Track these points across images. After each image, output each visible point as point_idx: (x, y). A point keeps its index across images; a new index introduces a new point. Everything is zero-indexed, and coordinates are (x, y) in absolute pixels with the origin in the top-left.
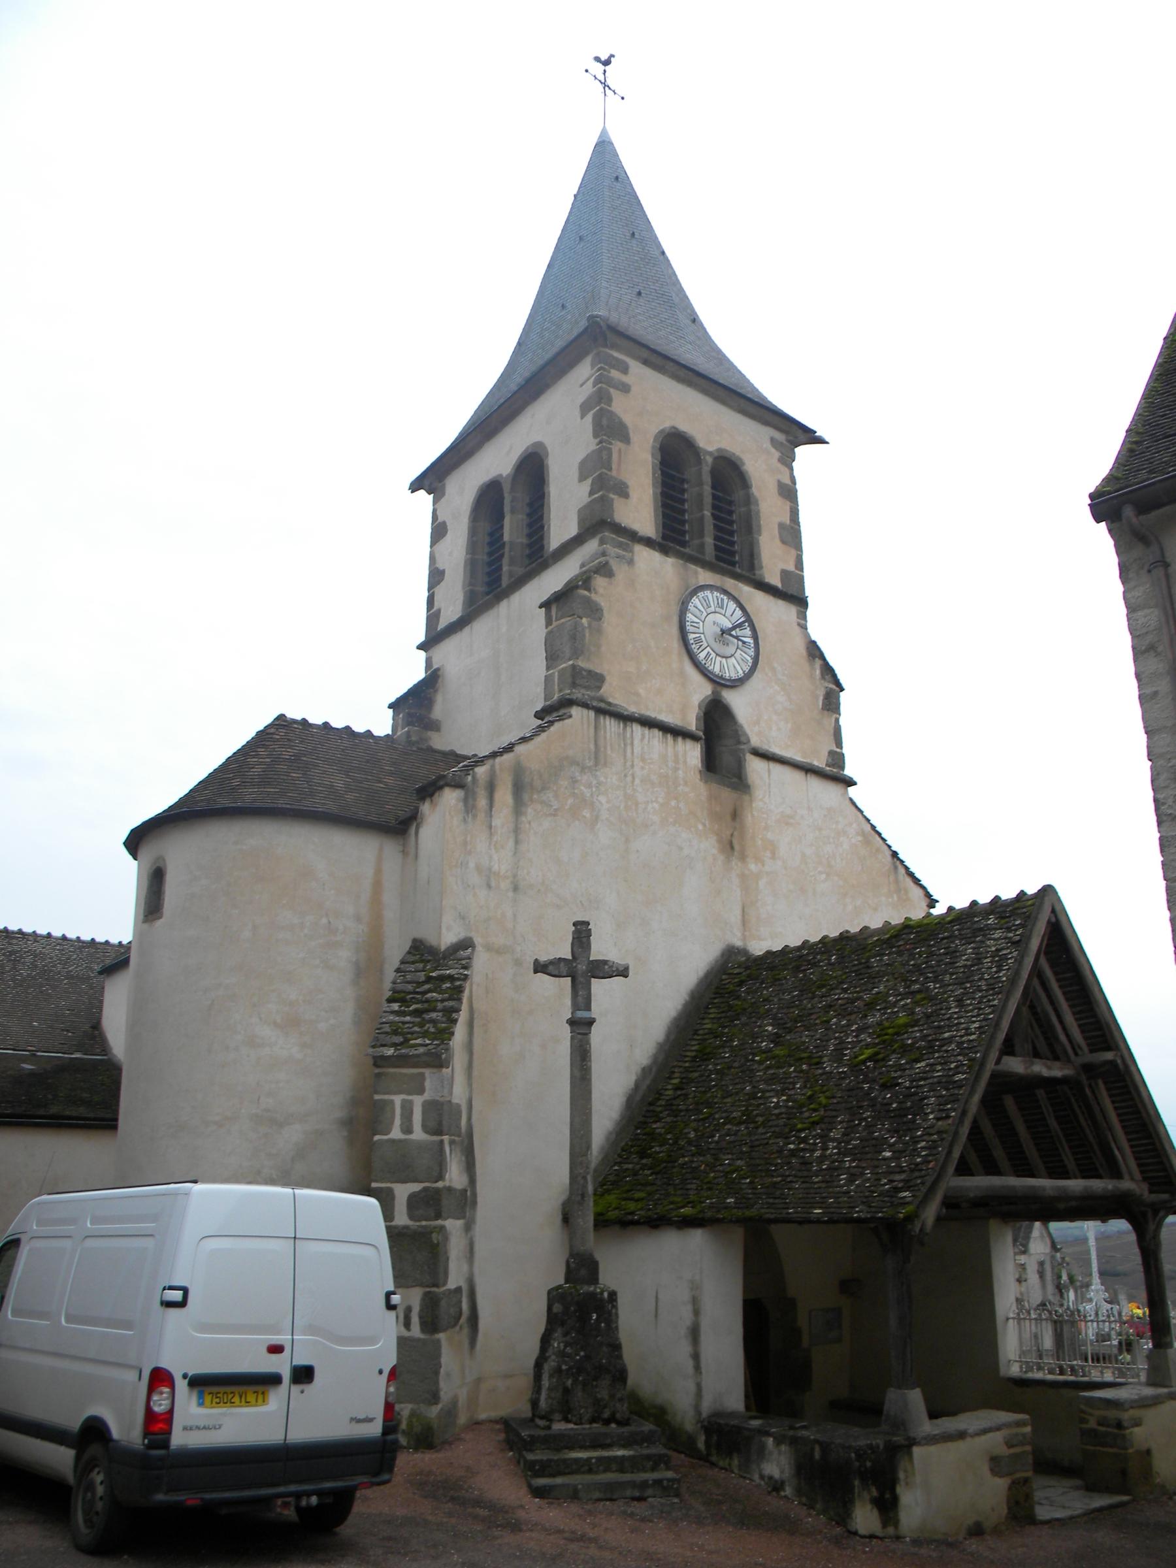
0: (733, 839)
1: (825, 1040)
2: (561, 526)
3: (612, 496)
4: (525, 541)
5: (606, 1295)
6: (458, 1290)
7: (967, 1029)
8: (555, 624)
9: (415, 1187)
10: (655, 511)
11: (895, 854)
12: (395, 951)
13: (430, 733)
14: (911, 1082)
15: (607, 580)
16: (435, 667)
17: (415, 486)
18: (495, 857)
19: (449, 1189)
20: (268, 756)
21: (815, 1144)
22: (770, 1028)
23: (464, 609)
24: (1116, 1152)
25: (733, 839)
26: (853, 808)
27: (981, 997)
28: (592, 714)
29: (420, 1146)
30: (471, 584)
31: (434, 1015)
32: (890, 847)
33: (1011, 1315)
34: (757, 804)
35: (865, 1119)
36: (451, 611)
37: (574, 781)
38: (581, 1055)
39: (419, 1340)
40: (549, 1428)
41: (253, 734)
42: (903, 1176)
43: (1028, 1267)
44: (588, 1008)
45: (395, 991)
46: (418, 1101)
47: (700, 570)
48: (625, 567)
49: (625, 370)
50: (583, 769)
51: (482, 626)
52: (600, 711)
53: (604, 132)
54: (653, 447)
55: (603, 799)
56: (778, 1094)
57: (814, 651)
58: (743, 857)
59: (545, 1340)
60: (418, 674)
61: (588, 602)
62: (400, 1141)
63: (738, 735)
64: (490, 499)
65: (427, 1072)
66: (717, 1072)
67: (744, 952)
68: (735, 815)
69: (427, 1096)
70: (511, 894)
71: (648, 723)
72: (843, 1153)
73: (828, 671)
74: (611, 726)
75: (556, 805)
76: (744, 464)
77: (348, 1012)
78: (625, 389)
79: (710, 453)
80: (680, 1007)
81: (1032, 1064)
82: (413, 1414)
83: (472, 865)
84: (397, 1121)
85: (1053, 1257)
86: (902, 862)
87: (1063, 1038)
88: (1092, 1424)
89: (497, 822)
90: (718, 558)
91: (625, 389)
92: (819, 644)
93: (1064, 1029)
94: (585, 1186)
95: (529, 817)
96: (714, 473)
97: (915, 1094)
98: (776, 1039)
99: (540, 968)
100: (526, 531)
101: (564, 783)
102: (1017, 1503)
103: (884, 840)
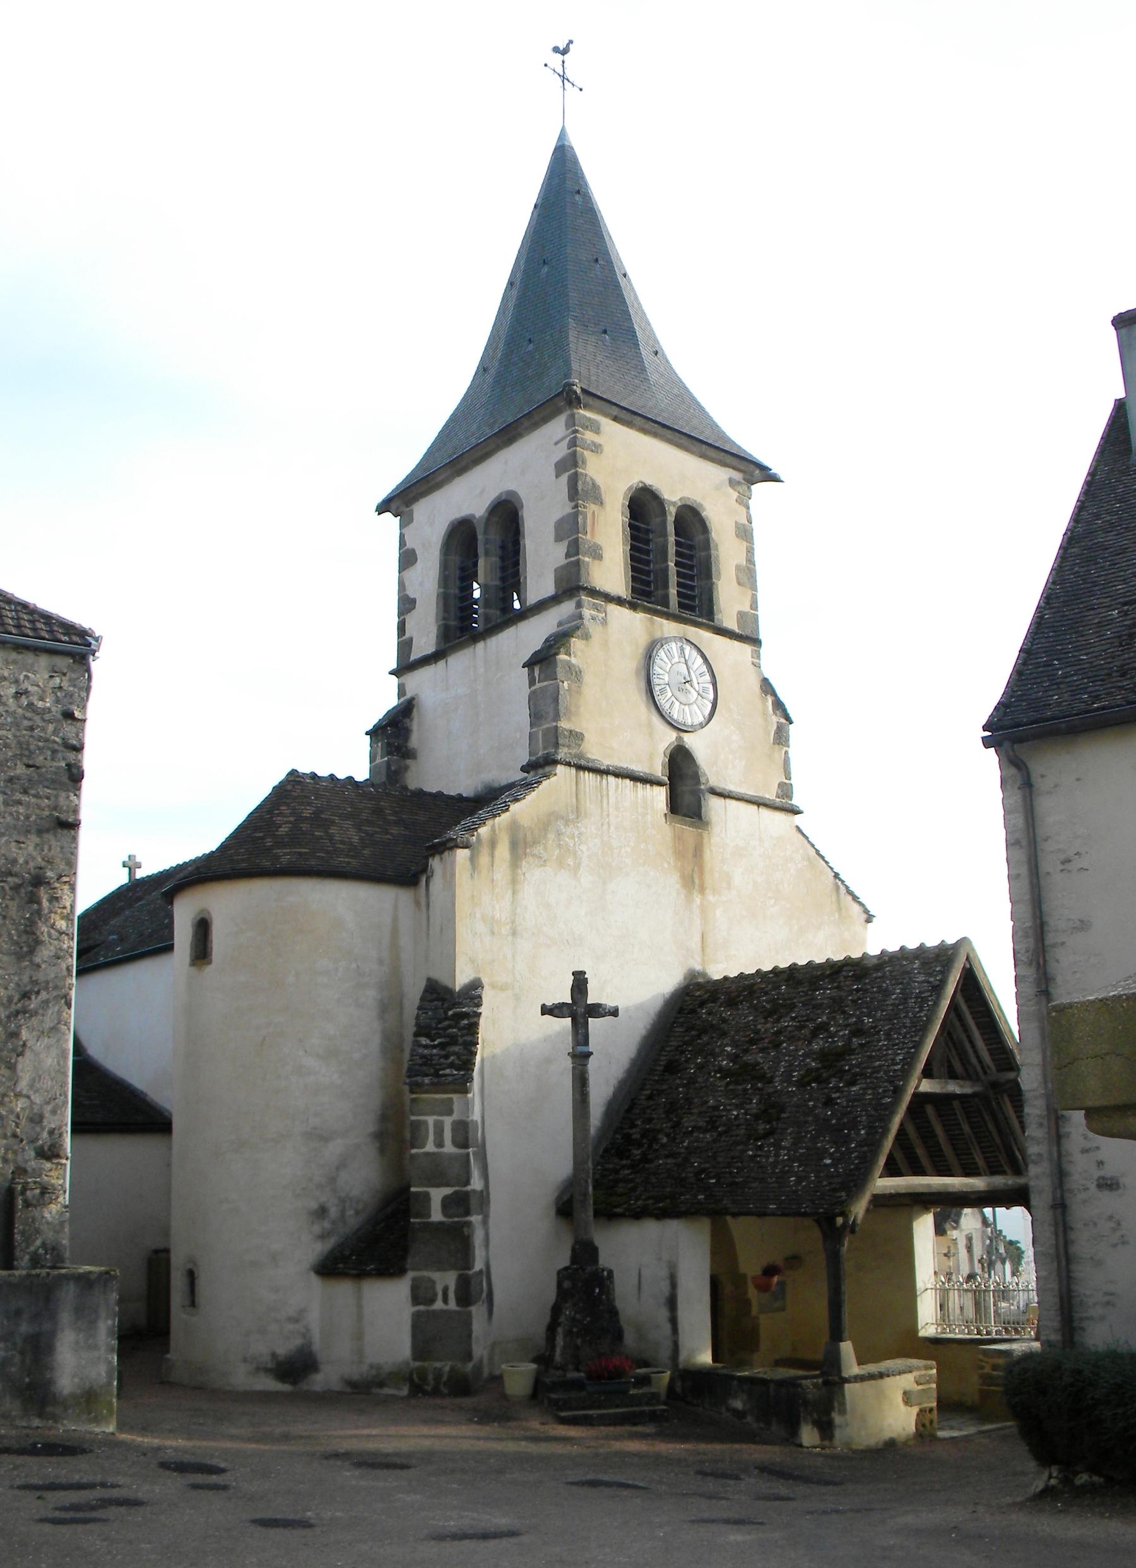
0: (693, 872)
1: (777, 1061)
2: (539, 581)
3: (587, 559)
4: (498, 583)
5: (605, 1273)
6: (481, 1271)
7: (893, 1060)
8: (538, 685)
9: (448, 1191)
10: (626, 564)
11: (836, 876)
12: (414, 992)
13: (408, 762)
14: (848, 1101)
15: (584, 642)
16: (408, 696)
17: (382, 508)
18: (497, 907)
19: (474, 1191)
20: (292, 814)
21: (770, 1151)
22: (729, 1049)
23: (438, 644)
24: (1017, 1153)
25: (693, 872)
26: (800, 836)
27: (906, 1033)
28: (573, 770)
29: (452, 1158)
30: (444, 619)
31: (456, 1049)
32: (832, 868)
33: (929, 1286)
34: (715, 840)
35: (810, 1132)
36: (425, 644)
37: (559, 834)
38: (581, 1081)
39: (455, 1312)
40: (564, 1376)
41: (270, 791)
42: (840, 1180)
43: (958, 1241)
44: (586, 1043)
45: (417, 1025)
46: (448, 1121)
47: (665, 622)
48: (600, 628)
49: (597, 430)
50: (567, 822)
51: (459, 661)
52: (580, 768)
53: (563, 135)
54: (623, 505)
55: (584, 848)
56: (738, 1107)
57: (767, 687)
58: (702, 890)
59: (556, 1310)
60: (391, 701)
61: (570, 667)
62: (434, 1154)
63: (696, 776)
64: (462, 538)
65: (455, 1097)
66: (683, 1086)
67: (703, 974)
68: (698, 851)
69: (456, 1116)
70: (510, 938)
71: (620, 774)
72: (792, 1160)
73: (779, 706)
74: (588, 777)
75: (545, 855)
76: (704, 510)
77: (376, 1042)
78: (596, 448)
79: (674, 504)
80: (649, 1027)
81: (947, 1084)
82: (452, 1369)
83: (478, 915)
84: (431, 1138)
85: (984, 1232)
86: (843, 882)
87: (974, 1061)
88: (987, 1370)
89: (498, 876)
90: (681, 605)
91: (596, 448)
92: (771, 681)
93: (976, 1052)
94: (587, 1188)
95: (524, 870)
96: (677, 522)
97: (850, 1112)
98: (734, 1058)
99: (546, 1010)
100: (499, 574)
101: (551, 836)
102: (924, 1425)
103: (827, 862)
